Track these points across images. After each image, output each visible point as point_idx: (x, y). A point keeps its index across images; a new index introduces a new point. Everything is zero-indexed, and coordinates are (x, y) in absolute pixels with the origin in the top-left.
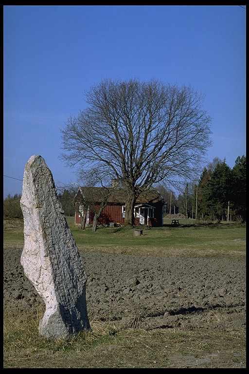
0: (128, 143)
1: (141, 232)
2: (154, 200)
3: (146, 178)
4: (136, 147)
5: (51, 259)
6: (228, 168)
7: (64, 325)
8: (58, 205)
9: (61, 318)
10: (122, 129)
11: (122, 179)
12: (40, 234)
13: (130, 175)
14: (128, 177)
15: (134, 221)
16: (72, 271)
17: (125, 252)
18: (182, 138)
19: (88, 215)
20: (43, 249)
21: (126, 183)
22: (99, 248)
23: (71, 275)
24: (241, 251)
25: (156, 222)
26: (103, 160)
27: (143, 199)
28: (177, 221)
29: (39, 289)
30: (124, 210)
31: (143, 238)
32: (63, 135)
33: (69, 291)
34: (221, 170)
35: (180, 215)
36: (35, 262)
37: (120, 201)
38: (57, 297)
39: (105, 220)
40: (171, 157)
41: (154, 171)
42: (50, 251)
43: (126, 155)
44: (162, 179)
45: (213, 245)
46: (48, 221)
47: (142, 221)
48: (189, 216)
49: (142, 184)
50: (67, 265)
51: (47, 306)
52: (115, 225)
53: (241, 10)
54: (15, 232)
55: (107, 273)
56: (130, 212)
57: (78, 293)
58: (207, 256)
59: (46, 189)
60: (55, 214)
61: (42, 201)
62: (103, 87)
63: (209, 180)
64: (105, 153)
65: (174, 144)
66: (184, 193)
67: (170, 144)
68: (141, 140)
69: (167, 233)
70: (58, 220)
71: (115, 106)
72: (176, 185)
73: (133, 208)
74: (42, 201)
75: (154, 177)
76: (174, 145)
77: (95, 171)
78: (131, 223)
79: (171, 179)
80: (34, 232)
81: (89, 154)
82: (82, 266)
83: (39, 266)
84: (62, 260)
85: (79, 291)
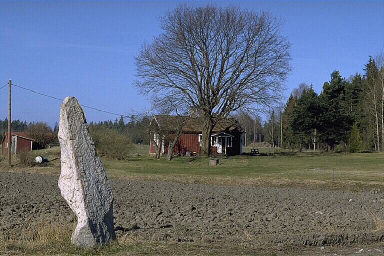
0: (205, 69)
2: (230, 127)
3: (223, 106)
5: (82, 182)
6: (316, 94)
10: (199, 56)
12: (73, 162)
13: (207, 102)
14: (205, 105)
15: (211, 151)
18: (260, 65)
19: (163, 144)
22: (170, 177)
23: (99, 195)
24: (317, 179)
25: (234, 151)
26: (179, 88)
27: (219, 128)
29: (72, 206)
30: (201, 139)
32: (135, 61)
33: (97, 208)
34: (308, 95)
35: (265, 144)
36: (69, 186)
38: (87, 213)
40: (249, 84)
42: (82, 176)
43: (203, 85)
44: (239, 106)
48: (276, 144)
51: (79, 220)
52: (192, 155)
56: (207, 141)
57: (105, 210)
59: (78, 124)
60: (86, 145)
61: (75, 134)
63: (294, 107)
64: (180, 80)
65: (252, 70)
66: (270, 121)
67: (247, 72)
68: (219, 67)
70: (89, 151)
71: (190, 32)
72: (261, 112)
73: (210, 137)
74: (75, 134)
75: (232, 105)
77: (170, 99)
78: (207, 151)
79: (250, 107)
81: (164, 81)
82: (109, 189)
83: (72, 188)
85: (106, 209)
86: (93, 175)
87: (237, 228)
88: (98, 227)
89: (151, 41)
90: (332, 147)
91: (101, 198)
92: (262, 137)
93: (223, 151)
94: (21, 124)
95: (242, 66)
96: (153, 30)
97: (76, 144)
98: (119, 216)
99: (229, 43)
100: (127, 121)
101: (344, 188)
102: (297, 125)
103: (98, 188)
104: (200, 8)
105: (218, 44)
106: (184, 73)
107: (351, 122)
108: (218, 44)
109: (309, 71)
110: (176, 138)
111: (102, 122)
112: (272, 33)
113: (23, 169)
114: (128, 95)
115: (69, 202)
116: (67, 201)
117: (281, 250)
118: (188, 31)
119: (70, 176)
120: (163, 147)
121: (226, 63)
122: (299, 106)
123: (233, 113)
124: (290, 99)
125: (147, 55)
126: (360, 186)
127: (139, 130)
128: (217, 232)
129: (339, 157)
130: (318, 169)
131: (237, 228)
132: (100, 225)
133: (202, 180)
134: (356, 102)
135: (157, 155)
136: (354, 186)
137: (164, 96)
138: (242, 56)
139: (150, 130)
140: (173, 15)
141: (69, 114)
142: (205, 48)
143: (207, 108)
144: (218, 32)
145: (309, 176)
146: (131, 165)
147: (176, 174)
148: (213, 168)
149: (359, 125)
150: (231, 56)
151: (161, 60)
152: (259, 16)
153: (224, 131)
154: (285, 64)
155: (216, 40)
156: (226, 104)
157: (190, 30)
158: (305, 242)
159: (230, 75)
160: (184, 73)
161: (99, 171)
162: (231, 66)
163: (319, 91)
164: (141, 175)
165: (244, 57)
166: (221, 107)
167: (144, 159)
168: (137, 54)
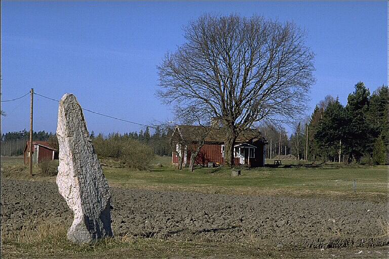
0: (228, 79)
1: (239, 173)
3: (246, 117)
4: (236, 85)
5: (79, 179)
7: (88, 232)
10: (222, 66)
11: (220, 118)
13: (230, 113)
15: (234, 162)
17: (219, 192)
20: (72, 170)
21: (225, 121)
23: (96, 192)
24: (337, 191)
25: (256, 162)
26: (202, 98)
27: (242, 138)
28: (279, 162)
30: (223, 150)
31: (240, 179)
32: (159, 71)
37: (218, 140)
39: (202, 159)
40: (272, 95)
41: (255, 109)
44: (262, 117)
45: (312, 185)
47: (242, 161)
48: (301, 156)
49: (242, 122)
50: (93, 184)
52: (214, 166)
54: (108, 171)
55: (187, 209)
57: (102, 207)
58: (302, 196)
59: (76, 121)
60: (83, 142)
62: (202, 22)
63: (320, 119)
64: (203, 91)
67: (270, 82)
68: (241, 78)
69: (267, 172)
75: (255, 116)
76: (276, 83)
77: (193, 109)
79: (273, 118)
80: (66, 157)
85: (103, 206)
86: (90, 172)
87: (244, 232)
89: (174, 50)
90: (358, 159)
91: (98, 195)
92: (288, 150)
93: (246, 162)
94: (47, 135)
95: (266, 76)
96: (174, 39)
98: (129, 220)
99: (252, 53)
100: (152, 132)
101: (364, 199)
102: (319, 136)
103: (95, 184)
104: (224, 18)
105: (242, 54)
106: (206, 83)
107: (375, 133)
108: (242, 54)
109: (331, 82)
110: (199, 149)
111: (127, 134)
112: (296, 43)
113: (44, 178)
114: (141, 97)
115: (67, 198)
116: (65, 197)
117: (279, 251)
118: (211, 42)
119: (68, 173)
120: (185, 159)
121: (249, 73)
122: (324, 119)
123: (256, 124)
124: (315, 111)
125: (170, 65)
126: (381, 197)
127: (160, 143)
128: (224, 235)
129: (363, 169)
130: (342, 182)
131: (244, 232)
132: (96, 221)
133: (222, 190)
134: (382, 115)
135: (179, 165)
136: (375, 197)
137: (186, 106)
138: (266, 66)
139: (172, 140)
140: (196, 24)
141: (67, 111)
142: (228, 58)
143: (230, 118)
144: (242, 42)
145: (332, 188)
146: (153, 175)
147: (197, 185)
148: (235, 178)
149: (383, 138)
150: (254, 66)
151: (184, 70)
152: (283, 27)
153: (247, 142)
154: (308, 74)
155: (240, 50)
156: (249, 115)
157: (214, 39)
158: (309, 246)
159: (252, 86)
160: (206, 83)
161: (96, 168)
162: (253, 77)
163: (344, 103)
164: (162, 185)
165: (267, 67)
166: (244, 117)
167: (168, 169)
168: (161, 63)
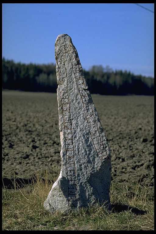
7: (65, 199)
8: (81, 82)
9: (62, 192)
16: (90, 146)
33: (80, 166)
46: (67, 97)
53: (151, 6)
57: (93, 168)
70: (79, 96)
74: (63, 78)
84: (79, 134)
85: (96, 166)
88: (78, 188)
91: (89, 154)
97: (63, 90)
132: (81, 185)
161: (91, 120)
